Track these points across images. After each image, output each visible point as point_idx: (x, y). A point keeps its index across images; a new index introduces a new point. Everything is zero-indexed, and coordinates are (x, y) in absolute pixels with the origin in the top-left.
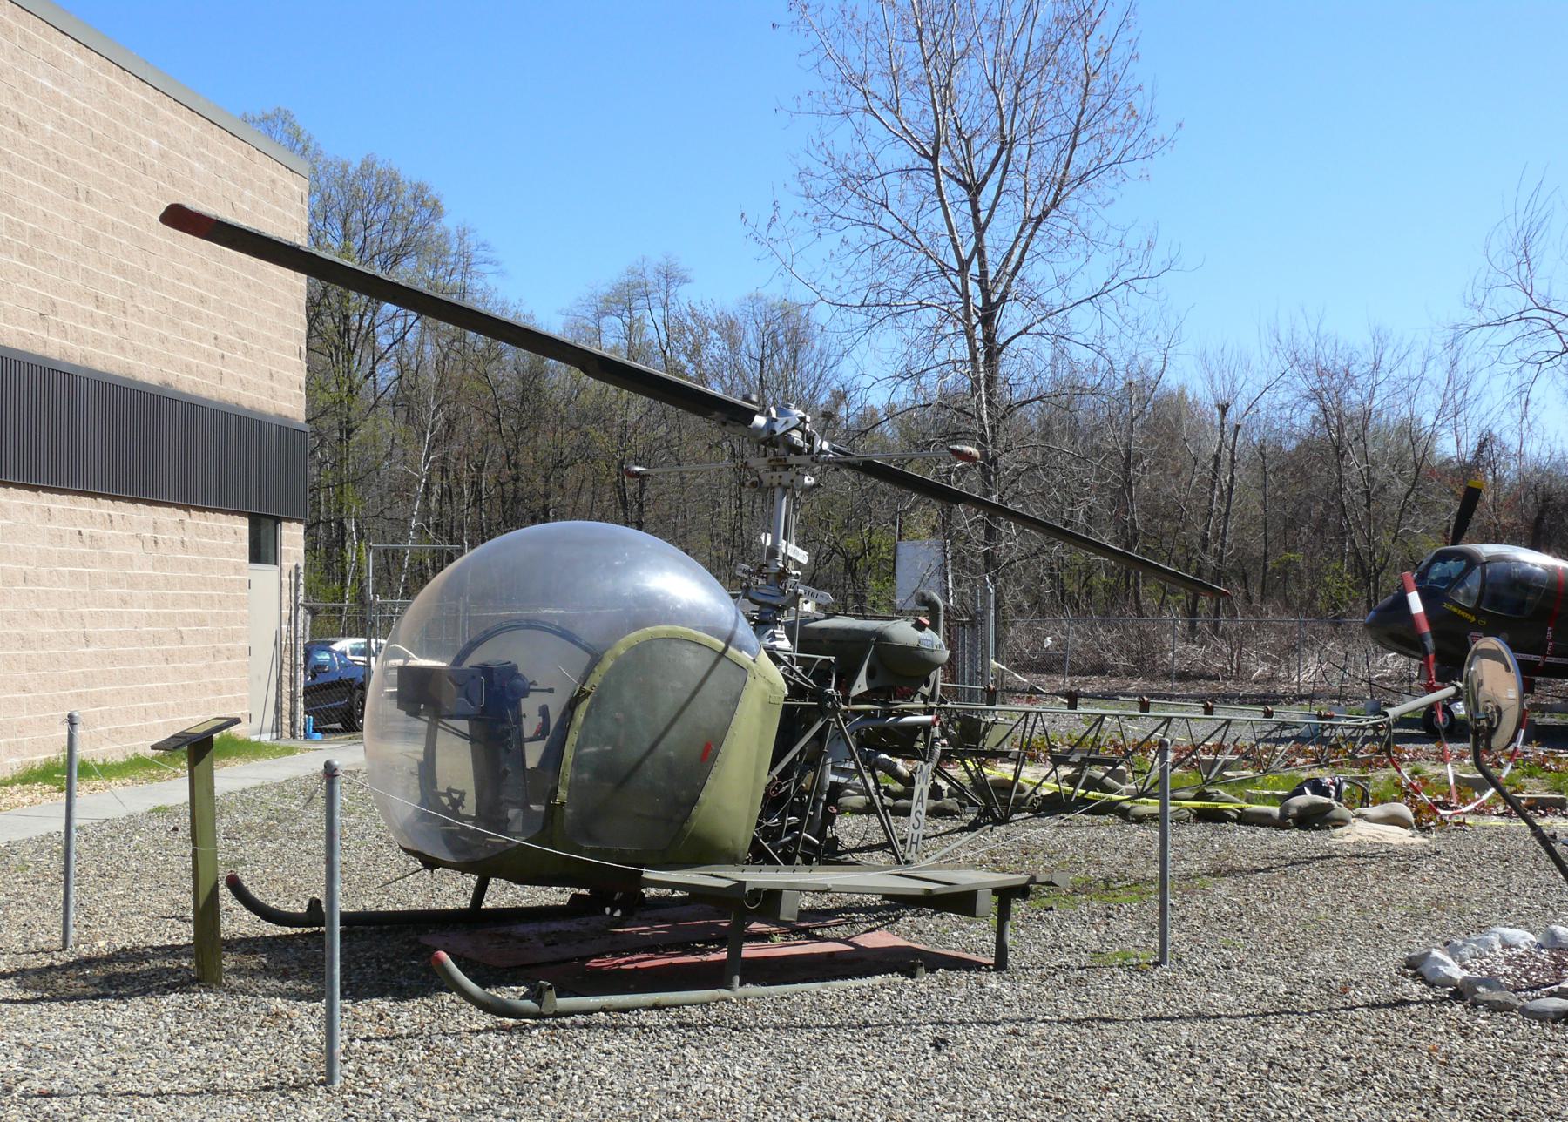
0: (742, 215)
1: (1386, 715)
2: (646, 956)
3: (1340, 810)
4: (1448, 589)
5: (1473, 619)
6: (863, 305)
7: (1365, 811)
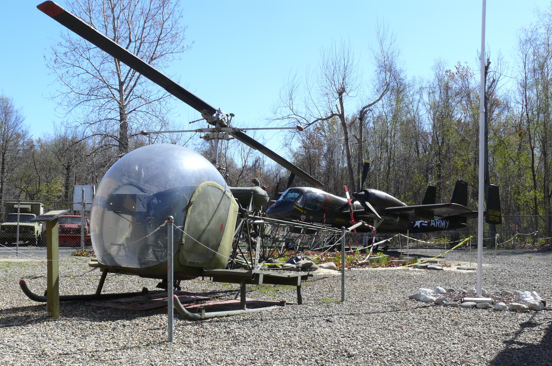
0: (44, 57)
1: (348, 230)
2: (187, 305)
3: (314, 265)
4: (295, 201)
5: (302, 211)
6: (88, 95)
7: (322, 265)
